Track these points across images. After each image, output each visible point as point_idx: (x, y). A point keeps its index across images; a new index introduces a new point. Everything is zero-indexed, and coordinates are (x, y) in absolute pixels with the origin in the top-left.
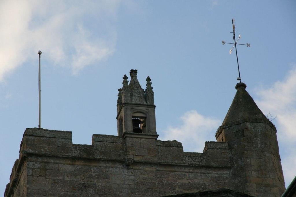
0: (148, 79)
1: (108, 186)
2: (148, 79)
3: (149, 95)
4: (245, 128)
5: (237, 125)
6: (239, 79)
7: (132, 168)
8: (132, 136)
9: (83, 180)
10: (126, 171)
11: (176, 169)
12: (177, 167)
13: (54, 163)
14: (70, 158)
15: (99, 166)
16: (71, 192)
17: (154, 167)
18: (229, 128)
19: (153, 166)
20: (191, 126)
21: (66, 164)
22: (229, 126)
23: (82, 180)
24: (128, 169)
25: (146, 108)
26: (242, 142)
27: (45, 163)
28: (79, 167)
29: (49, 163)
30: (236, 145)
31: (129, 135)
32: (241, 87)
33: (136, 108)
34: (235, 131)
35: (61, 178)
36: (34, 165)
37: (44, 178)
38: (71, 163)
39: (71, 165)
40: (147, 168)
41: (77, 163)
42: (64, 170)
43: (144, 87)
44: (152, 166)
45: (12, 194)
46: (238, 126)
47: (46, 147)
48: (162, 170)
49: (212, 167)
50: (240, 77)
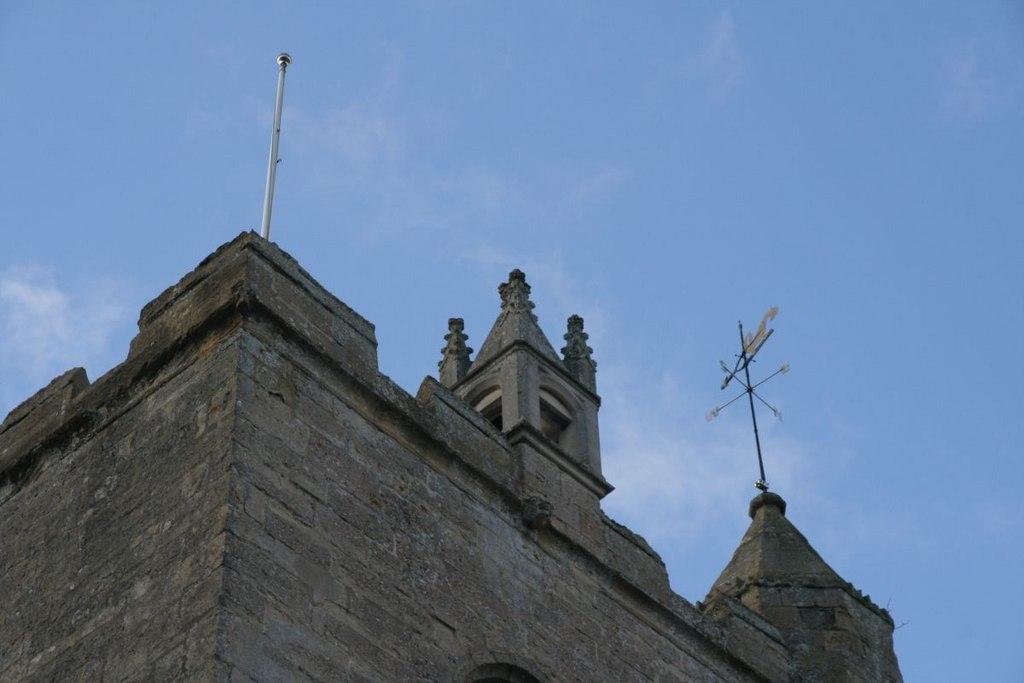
0: (576, 323)
1: (471, 552)
2: (576, 323)
3: (576, 365)
4: (841, 606)
5: (808, 587)
6: (761, 487)
7: (537, 543)
8: (542, 447)
9: (402, 489)
10: (520, 540)
11: (652, 617)
12: (656, 614)
13: (322, 386)
14: (375, 395)
15: (448, 478)
16: (366, 505)
17: (594, 577)
18: (779, 591)
19: (594, 573)
21: (355, 411)
22: (779, 582)
23: (397, 488)
24: (526, 536)
25: (578, 393)
26: (826, 644)
27: (297, 366)
28: (392, 443)
29: (306, 374)
30: (805, 647)
31: (531, 439)
32: (769, 505)
33: (553, 375)
34: (801, 604)
35: (340, 444)
36: (262, 351)
37: (289, 410)
38: (370, 416)
39: (369, 422)
40: (577, 568)
41: (385, 426)
42: (348, 425)
43: (558, 342)
44: (591, 573)
45: (15, 481)
46: (813, 593)
47: (304, 322)
48: (617, 601)
49: (750, 670)
50: (763, 478)
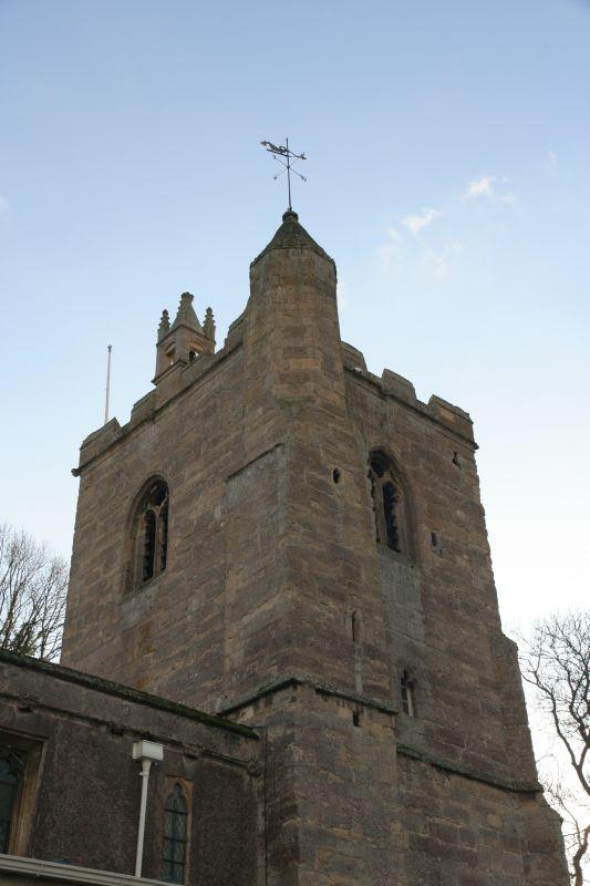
20: (225, 301)
32: (290, 217)
